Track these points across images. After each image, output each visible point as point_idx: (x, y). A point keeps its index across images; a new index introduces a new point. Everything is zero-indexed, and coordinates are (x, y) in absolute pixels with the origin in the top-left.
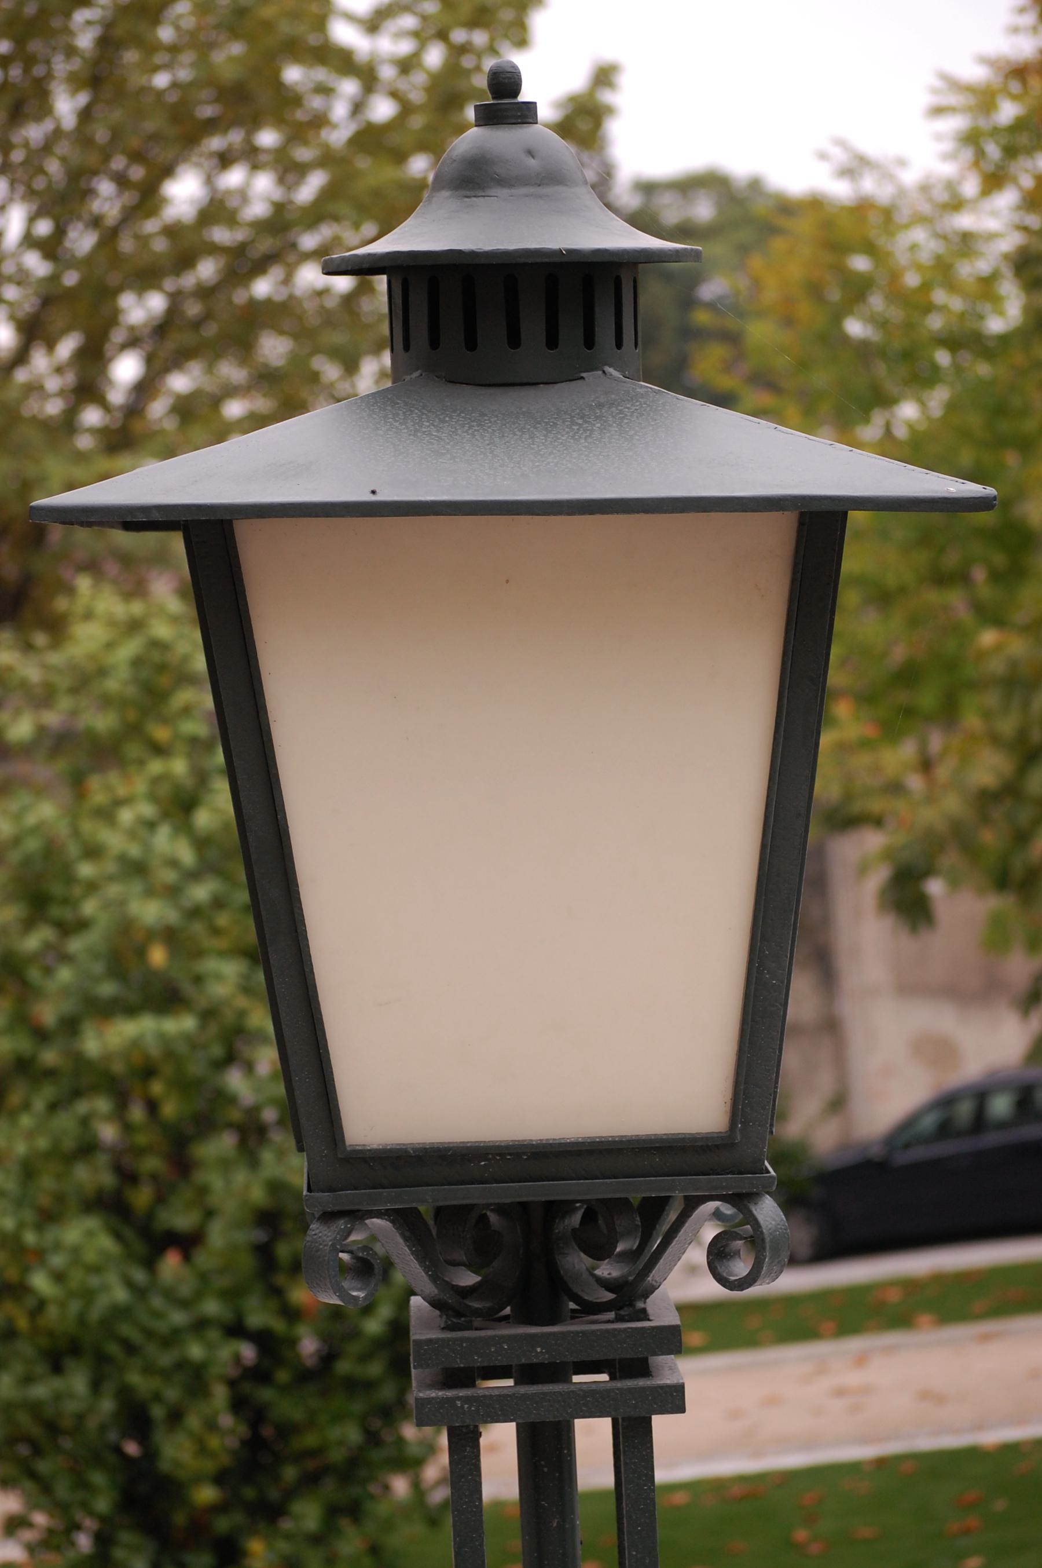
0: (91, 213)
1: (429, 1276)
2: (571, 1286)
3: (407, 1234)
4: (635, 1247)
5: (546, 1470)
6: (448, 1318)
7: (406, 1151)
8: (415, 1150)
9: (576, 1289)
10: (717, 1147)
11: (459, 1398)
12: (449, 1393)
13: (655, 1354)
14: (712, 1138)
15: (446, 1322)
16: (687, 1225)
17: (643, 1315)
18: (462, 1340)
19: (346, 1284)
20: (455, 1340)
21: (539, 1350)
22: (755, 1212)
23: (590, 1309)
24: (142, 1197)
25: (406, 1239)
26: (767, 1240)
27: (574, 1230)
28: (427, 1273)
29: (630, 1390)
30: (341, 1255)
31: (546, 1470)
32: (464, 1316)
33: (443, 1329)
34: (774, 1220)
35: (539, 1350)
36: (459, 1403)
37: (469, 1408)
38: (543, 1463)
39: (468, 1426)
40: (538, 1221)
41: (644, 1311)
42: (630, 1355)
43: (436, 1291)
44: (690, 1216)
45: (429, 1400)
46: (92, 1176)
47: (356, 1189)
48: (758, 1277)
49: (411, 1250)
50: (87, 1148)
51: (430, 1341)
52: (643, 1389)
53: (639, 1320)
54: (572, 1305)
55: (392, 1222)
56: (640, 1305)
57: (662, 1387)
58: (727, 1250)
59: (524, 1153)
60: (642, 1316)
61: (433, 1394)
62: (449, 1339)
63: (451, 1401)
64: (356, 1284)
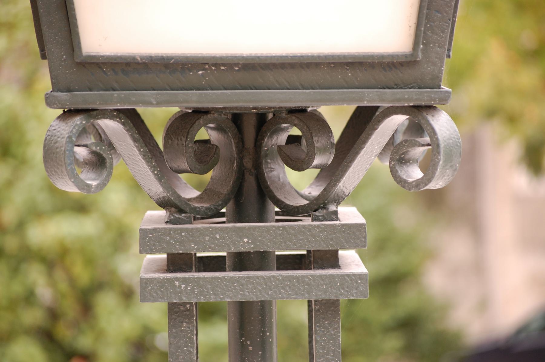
0: (224, 318)
1: (155, 174)
2: (276, 194)
3: (137, 136)
4: (330, 162)
5: (251, 348)
6: (171, 214)
7: (134, 58)
8: (142, 58)
9: (280, 196)
10: (402, 64)
11: (177, 279)
12: (170, 275)
13: (344, 248)
14: (398, 56)
15: (169, 217)
16: (373, 137)
17: (335, 215)
18: (182, 230)
19: (82, 176)
20: (175, 230)
21: (246, 240)
22: (432, 122)
23: (290, 211)
24: (64, 332)
25: (135, 140)
26: (442, 145)
27: (279, 147)
28: (153, 172)
29: (321, 277)
30: (76, 149)
31: (251, 348)
32: (185, 212)
33: (167, 222)
34: (448, 130)
35: (246, 240)
36: (177, 283)
37: (186, 288)
38: (249, 342)
39: (184, 304)
40: (250, 130)
41: (335, 213)
42: (323, 247)
43: (161, 189)
44: (376, 129)
45: (152, 280)
46: (32, 317)
47: (91, 90)
48: (433, 177)
49: (139, 150)
50: (29, 298)
51: (154, 230)
52: (333, 276)
53: (332, 220)
54: (277, 209)
55: (123, 124)
56: (332, 208)
57: (348, 275)
58: (407, 157)
59: (237, 65)
60: (334, 217)
61: (156, 275)
62: (170, 229)
63: (171, 281)
64: (92, 175)
